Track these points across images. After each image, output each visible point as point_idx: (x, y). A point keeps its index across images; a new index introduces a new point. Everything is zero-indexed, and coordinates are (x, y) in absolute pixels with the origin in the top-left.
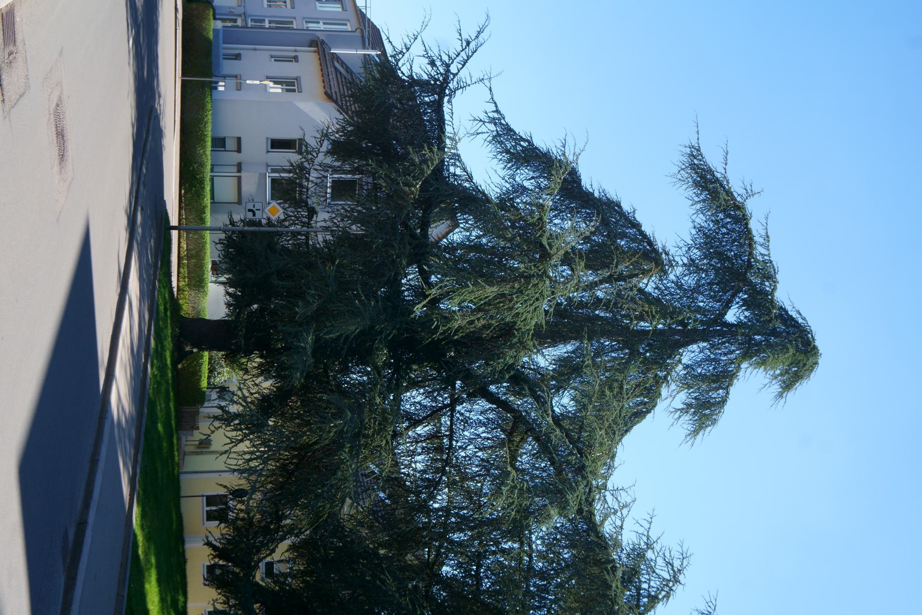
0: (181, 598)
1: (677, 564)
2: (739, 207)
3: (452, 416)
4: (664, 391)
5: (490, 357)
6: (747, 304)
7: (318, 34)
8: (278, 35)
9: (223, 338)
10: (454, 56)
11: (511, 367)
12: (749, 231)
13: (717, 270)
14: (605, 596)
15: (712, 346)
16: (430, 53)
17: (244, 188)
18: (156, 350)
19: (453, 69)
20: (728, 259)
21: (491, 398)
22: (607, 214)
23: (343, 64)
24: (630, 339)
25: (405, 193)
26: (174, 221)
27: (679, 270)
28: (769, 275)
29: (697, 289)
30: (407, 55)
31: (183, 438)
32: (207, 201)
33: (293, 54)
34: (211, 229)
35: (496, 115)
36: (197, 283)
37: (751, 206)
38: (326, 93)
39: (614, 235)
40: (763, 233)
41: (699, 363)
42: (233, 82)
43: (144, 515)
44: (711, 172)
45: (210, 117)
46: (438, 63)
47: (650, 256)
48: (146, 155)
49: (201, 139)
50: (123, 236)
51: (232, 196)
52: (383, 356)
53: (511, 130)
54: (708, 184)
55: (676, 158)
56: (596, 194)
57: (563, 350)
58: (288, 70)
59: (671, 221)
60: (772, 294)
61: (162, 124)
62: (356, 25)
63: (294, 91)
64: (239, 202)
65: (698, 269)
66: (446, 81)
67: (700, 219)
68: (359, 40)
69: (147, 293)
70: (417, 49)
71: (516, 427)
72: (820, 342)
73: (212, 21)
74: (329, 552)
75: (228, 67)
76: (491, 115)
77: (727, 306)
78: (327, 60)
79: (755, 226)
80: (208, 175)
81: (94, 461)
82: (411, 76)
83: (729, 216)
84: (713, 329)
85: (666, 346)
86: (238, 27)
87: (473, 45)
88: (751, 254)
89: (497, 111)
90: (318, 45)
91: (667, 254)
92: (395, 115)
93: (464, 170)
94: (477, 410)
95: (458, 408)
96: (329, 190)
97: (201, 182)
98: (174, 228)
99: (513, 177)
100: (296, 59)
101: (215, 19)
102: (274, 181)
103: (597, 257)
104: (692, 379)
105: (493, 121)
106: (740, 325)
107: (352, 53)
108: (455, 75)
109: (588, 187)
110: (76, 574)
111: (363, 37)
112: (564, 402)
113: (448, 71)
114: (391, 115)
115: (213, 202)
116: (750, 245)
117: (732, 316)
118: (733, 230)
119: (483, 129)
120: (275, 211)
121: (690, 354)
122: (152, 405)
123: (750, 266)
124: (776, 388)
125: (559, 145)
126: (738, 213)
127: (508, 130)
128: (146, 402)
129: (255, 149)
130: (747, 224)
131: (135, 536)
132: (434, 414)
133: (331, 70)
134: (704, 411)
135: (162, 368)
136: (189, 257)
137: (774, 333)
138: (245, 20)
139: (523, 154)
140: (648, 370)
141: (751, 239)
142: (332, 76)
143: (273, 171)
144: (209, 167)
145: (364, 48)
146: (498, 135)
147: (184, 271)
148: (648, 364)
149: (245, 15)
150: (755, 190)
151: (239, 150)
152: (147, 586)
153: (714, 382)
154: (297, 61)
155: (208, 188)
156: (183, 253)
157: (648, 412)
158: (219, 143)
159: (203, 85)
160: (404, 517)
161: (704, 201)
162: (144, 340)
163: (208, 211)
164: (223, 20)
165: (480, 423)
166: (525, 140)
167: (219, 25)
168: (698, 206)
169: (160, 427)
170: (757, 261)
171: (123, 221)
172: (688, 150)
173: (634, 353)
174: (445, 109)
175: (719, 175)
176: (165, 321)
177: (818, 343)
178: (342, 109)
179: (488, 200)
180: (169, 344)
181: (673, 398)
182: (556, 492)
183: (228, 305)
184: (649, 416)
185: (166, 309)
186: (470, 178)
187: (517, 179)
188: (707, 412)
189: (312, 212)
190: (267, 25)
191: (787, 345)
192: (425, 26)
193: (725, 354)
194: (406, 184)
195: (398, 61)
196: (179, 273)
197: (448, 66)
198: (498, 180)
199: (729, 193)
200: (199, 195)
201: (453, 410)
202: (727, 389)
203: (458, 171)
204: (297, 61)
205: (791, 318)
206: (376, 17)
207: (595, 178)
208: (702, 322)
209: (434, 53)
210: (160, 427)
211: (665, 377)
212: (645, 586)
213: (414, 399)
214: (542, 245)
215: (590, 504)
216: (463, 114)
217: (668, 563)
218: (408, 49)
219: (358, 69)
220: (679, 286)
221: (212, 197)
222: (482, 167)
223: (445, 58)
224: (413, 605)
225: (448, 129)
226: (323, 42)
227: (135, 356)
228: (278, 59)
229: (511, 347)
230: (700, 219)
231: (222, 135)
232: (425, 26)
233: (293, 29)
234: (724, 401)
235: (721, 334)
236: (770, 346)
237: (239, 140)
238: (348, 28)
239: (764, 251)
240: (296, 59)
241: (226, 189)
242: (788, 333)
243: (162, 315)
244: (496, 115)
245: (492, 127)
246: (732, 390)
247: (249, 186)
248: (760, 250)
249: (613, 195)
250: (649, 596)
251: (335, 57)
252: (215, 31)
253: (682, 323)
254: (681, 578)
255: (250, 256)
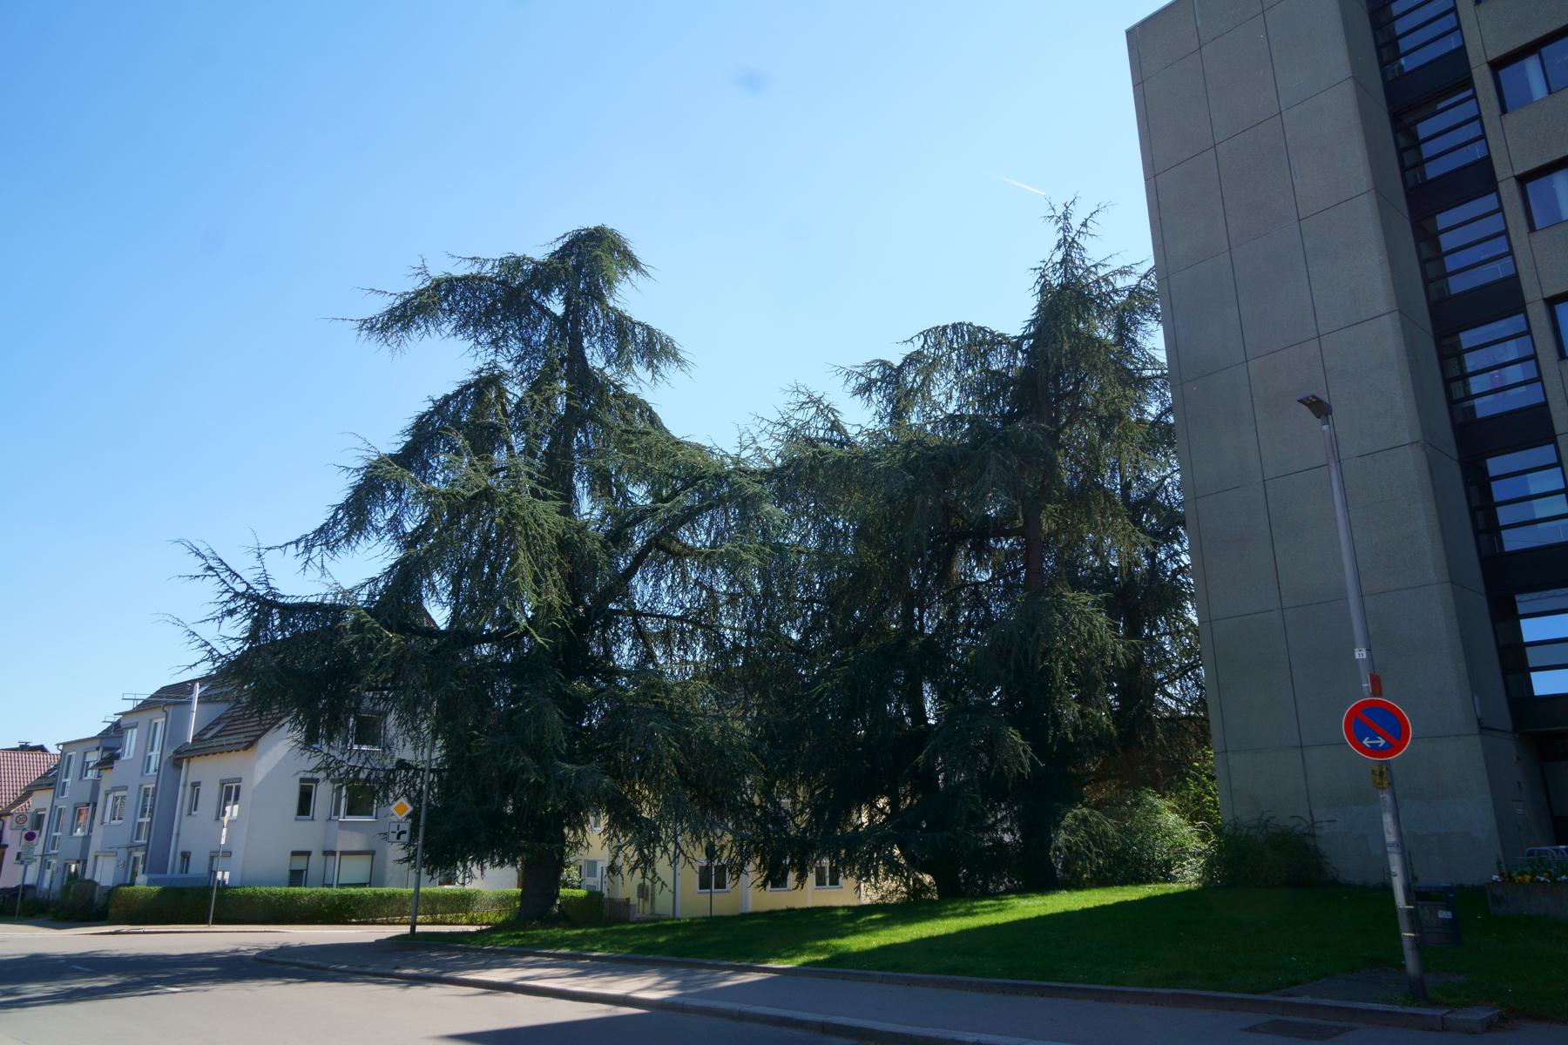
0: (840, 912)
1: (803, 398)
2: (437, 285)
3: (646, 615)
4: (630, 390)
5: (591, 566)
6: (547, 291)
7: (165, 757)
8: (162, 807)
9: (542, 873)
10: (225, 587)
11: (604, 545)
12: (466, 278)
13: (505, 318)
14: (848, 467)
15: (588, 333)
16: (218, 614)
17: (357, 848)
18: (571, 946)
19: (241, 588)
20: (494, 304)
21: (630, 573)
22: (426, 435)
23: (207, 729)
24: (574, 419)
25: (397, 651)
26: (406, 929)
27: (500, 359)
28: (514, 264)
29: (526, 341)
30: (215, 644)
31: (638, 915)
32: (367, 891)
33: (189, 787)
34: (418, 886)
35: (302, 544)
36: (463, 903)
37: (439, 270)
38: (246, 749)
39: (459, 421)
40: (469, 263)
41: (606, 350)
42: (220, 862)
43: (777, 955)
44: (391, 312)
45: (263, 889)
46: (232, 605)
47: (485, 385)
48: (323, 964)
49: (291, 899)
50: (436, 990)
51: (364, 862)
52: (581, 686)
53: (322, 529)
54: (408, 314)
55: (374, 349)
56: (408, 439)
57: (581, 487)
58: (210, 794)
59: (446, 360)
60: (537, 263)
61: (272, 947)
62: (159, 712)
63: (238, 789)
64: (372, 853)
65: (504, 337)
66: (256, 598)
67: (447, 328)
68: (178, 708)
69: (502, 958)
70: (209, 632)
71: (664, 548)
72: (591, 223)
73: (137, 887)
74: (781, 749)
75: (197, 868)
76: (301, 550)
77: (546, 312)
78: (203, 746)
79: (460, 270)
80: (335, 891)
81: (741, 1017)
82: (245, 640)
83: (446, 296)
84: (570, 329)
85: (584, 381)
86: (145, 857)
87: (213, 563)
88: (491, 279)
89: (297, 543)
90: (180, 757)
91: (481, 370)
92: (292, 662)
93: (363, 586)
94: (642, 589)
95: (638, 607)
96: (364, 748)
97: (343, 898)
98: (413, 929)
99: (377, 530)
100: (195, 785)
101: (132, 884)
102: (350, 812)
103: (484, 439)
104: (620, 359)
105: (308, 549)
106: (567, 301)
107: (194, 719)
108: (249, 587)
109: (399, 447)
110: (891, 1033)
111: (175, 704)
112: (639, 493)
113: (243, 595)
114: (293, 669)
115: (370, 884)
116: (482, 279)
117: (557, 307)
118: (463, 294)
119: (317, 560)
120: (399, 810)
121: (595, 358)
122: (640, 949)
123: (504, 282)
124: (633, 274)
125: (345, 474)
126: (443, 286)
127: (322, 531)
128: (640, 956)
129: (308, 835)
130: (457, 279)
131: (805, 964)
132: (640, 634)
133: (215, 742)
134: (656, 349)
135: (593, 939)
136: (433, 912)
137: (577, 268)
138: (137, 847)
139: (355, 514)
140: (608, 404)
141: (474, 277)
142: (224, 741)
143: (337, 813)
144: (326, 890)
145: (190, 703)
146: (327, 543)
147: (449, 917)
148: (602, 402)
149: (131, 847)
150: (419, 264)
151: (308, 854)
152: (854, 948)
153: (626, 335)
154: (199, 784)
155: (353, 890)
156: (429, 918)
157: (650, 410)
158: (296, 877)
159: (220, 898)
160: (752, 671)
161: (426, 321)
162: (561, 961)
163: (379, 890)
164: (134, 874)
165: (656, 585)
166: (336, 514)
167: (141, 879)
168: (432, 329)
169: (661, 940)
170: (499, 275)
171: (417, 992)
172: (365, 333)
173: (592, 416)
174: (289, 601)
175: (398, 302)
176: (532, 937)
177: (592, 226)
178: (275, 723)
179: (400, 562)
180: (557, 932)
181: (639, 382)
182: (748, 504)
183: (501, 864)
184: (655, 409)
185: (517, 937)
186: (374, 580)
187: (381, 525)
188: (658, 347)
189: (402, 764)
190: (147, 820)
191: (590, 259)
192: (178, 622)
193: (597, 321)
194: (387, 650)
195: (221, 656)
196: (451, 924)
197: (237, 594)
198: (380, 547)
199: (419, 293)
200: (359, 901)
201: (640, 614)
202: (634, 324)
203: (365, 592)
204: (199, 784)
205: (563, 248)
206: (148, 690)
207: (391, 441)
208: (562, 339)
209: (218, 610)
210: (661, 940)
211: (616, 387)
212: (821, 433)
213: (625, 654)
214: (474, 497)
215: (754, 473)
216: (300, 583)
217: (801, 407)
218: (207, 644)
219: (219, 709)
220: (520, 360)
221: (363, 885)
222: (364, 564)
223: (227, 596)
224: (843, 664)
225: (312, 600)
226: (177, 752)
227: (586, 972)
228: (194, 806)
229: (582, 542)
230: (447, 328)
231: (287, 874)
232: (178, 622)
233: (155, 790)
234: (649, 330)
235: (576, 323)
236: (592, 274)
237: (294, 854)
238: (161, 721)
239: (488, 266)
240: (195, 785)
241: (354, 869)
242: (579, 254)
243: (525, 941)
244: (302, 544)
245: (316, 550)
246: (636, 318)
247: (355, 842)
248: (487, 270)
249: (408, 422)
250: (831, 430)
251: (197, 738)
252: (149, 883)
253: (563, 360)
254: (817, 395)
255: (443, 843)
